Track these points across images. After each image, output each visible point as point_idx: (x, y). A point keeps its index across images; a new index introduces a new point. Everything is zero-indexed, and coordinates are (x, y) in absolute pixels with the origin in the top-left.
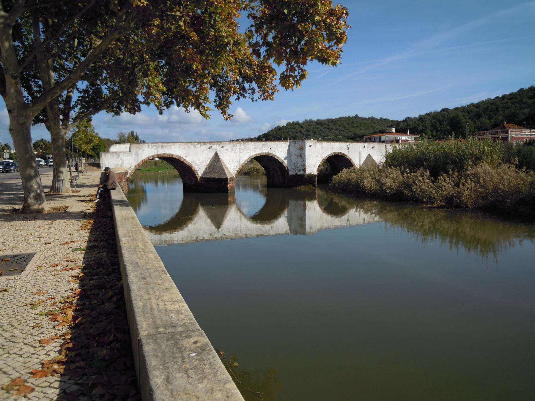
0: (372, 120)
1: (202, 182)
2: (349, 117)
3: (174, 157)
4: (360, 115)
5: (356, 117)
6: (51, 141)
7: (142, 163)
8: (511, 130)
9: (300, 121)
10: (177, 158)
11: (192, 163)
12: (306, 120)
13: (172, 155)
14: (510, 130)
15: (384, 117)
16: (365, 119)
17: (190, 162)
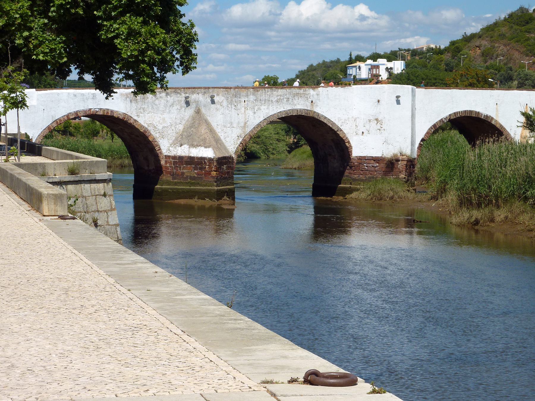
10: (121, 117)
11: (149, 128)
13: (112, 111)
17: (146, 126)
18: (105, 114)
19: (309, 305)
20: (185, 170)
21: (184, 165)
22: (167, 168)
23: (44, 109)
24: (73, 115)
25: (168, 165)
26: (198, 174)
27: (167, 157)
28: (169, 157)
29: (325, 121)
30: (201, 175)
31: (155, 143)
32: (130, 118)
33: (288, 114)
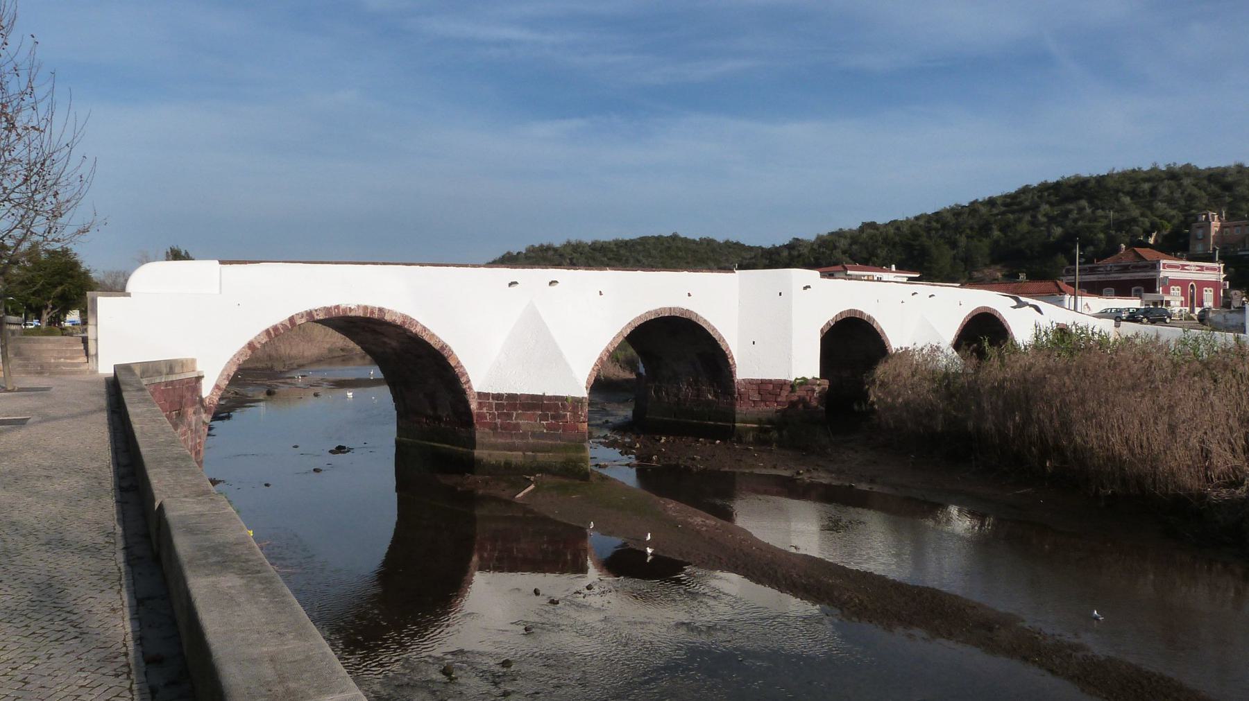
0: (708, 245)
1: (485, 410)
2: (661, 236)
3: (387, 318)
4: (688, 237)
5: (674, 237)
6: (383, 377)
7: (265, 340)
8: (1165, 261)
9: (557, 244)
10: (399, 322)
12: (569, 243)
14: (1162, 262)
15: (734, 239)
16: (694, 241)
18: (368, 315)
19: (12, 176)
20: (521, 420)
21: (520, 411)
22: (481, 416)
23: (960, 304)
24: (302, 317)
25: (485, 410)
26: (549, 427)
27: (481, 395)
28: (487, 395)
29: (704, 326)
30: (555, 429)
31: (461, 370)
33: (659, 315)
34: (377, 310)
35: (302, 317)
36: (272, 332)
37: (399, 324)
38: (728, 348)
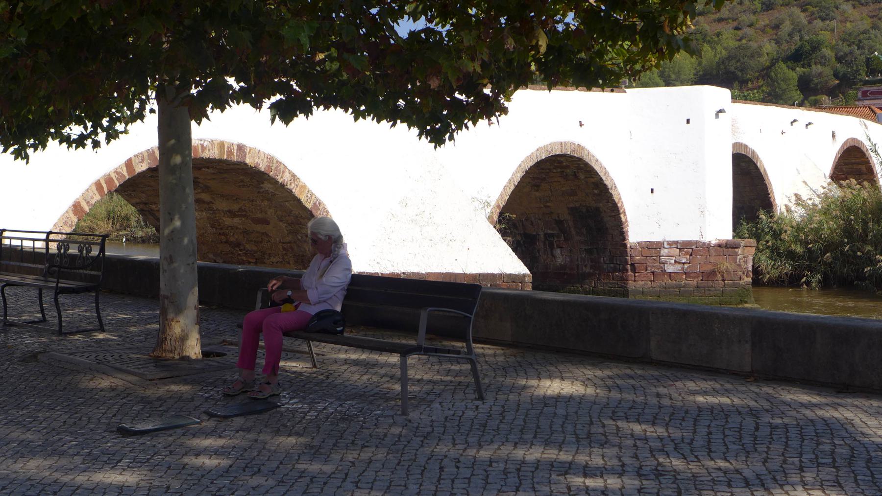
10: (262, 168)
18: (225, 157)
24: (143, 161)
29: (597, 168)
32: (282, 166)
33: (550, 152)
34: (235, 147)
35: (143, 161)
36: (105, 186)
37: (263, 170)
38: (620, 199)
